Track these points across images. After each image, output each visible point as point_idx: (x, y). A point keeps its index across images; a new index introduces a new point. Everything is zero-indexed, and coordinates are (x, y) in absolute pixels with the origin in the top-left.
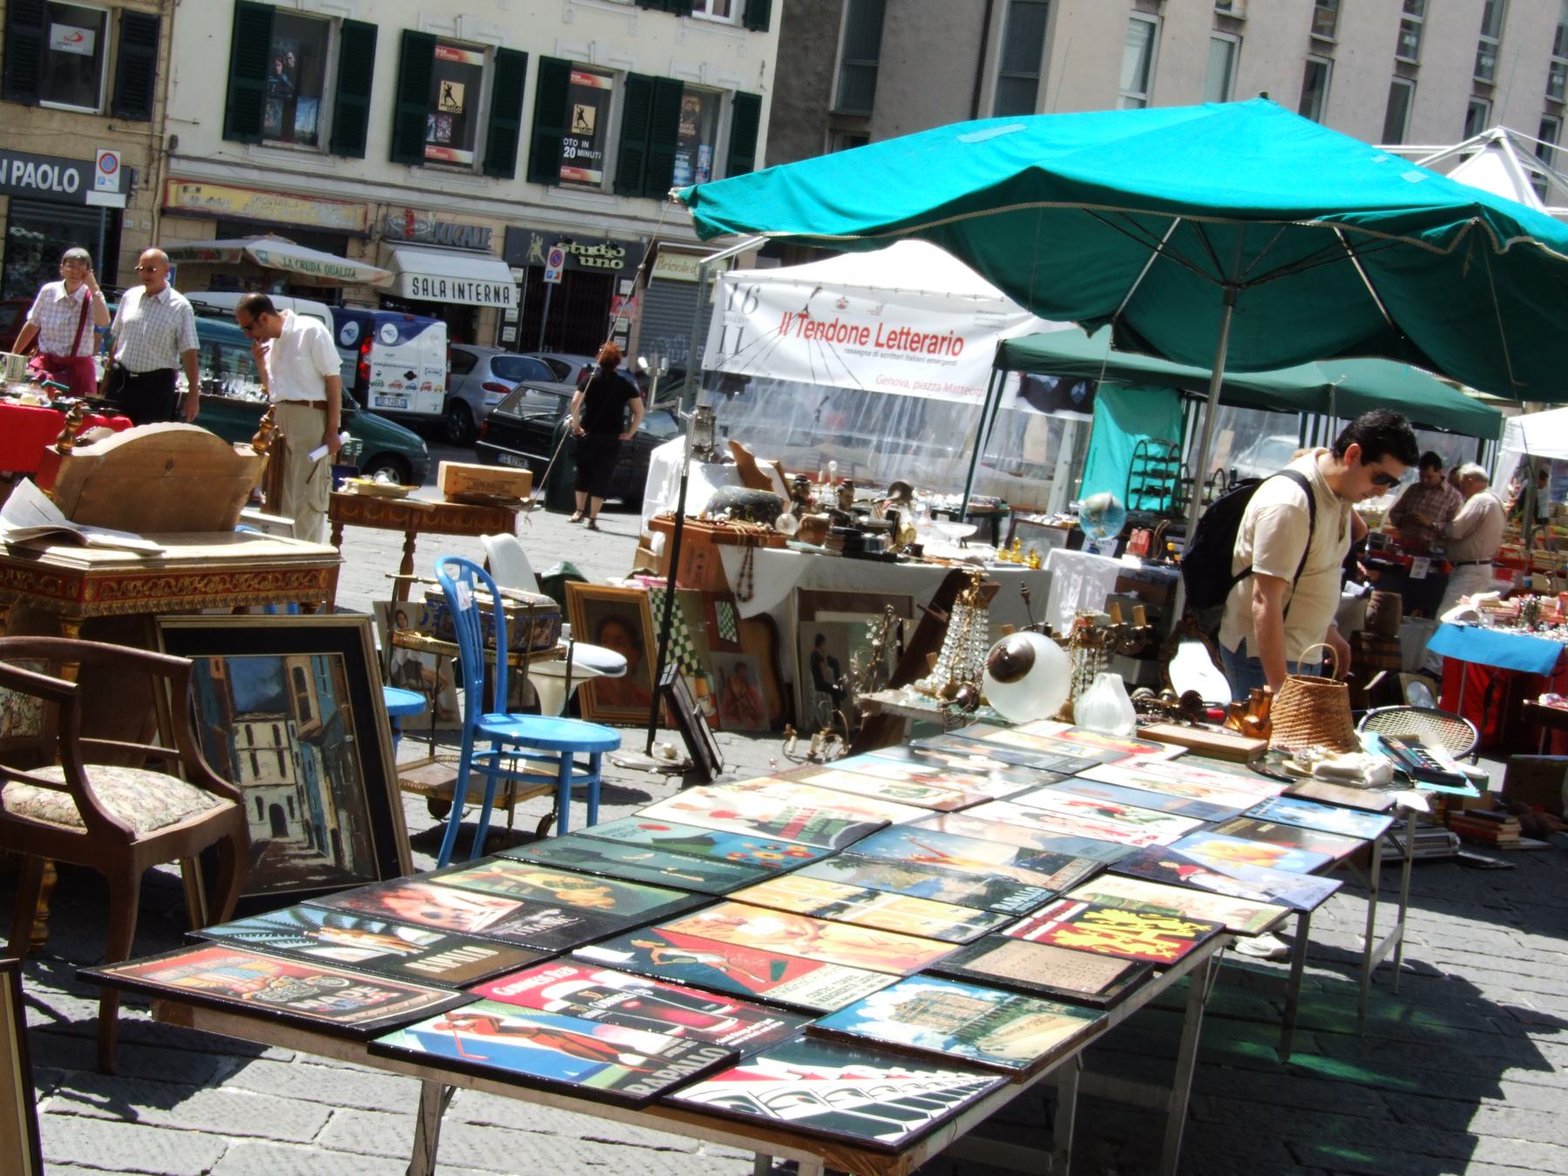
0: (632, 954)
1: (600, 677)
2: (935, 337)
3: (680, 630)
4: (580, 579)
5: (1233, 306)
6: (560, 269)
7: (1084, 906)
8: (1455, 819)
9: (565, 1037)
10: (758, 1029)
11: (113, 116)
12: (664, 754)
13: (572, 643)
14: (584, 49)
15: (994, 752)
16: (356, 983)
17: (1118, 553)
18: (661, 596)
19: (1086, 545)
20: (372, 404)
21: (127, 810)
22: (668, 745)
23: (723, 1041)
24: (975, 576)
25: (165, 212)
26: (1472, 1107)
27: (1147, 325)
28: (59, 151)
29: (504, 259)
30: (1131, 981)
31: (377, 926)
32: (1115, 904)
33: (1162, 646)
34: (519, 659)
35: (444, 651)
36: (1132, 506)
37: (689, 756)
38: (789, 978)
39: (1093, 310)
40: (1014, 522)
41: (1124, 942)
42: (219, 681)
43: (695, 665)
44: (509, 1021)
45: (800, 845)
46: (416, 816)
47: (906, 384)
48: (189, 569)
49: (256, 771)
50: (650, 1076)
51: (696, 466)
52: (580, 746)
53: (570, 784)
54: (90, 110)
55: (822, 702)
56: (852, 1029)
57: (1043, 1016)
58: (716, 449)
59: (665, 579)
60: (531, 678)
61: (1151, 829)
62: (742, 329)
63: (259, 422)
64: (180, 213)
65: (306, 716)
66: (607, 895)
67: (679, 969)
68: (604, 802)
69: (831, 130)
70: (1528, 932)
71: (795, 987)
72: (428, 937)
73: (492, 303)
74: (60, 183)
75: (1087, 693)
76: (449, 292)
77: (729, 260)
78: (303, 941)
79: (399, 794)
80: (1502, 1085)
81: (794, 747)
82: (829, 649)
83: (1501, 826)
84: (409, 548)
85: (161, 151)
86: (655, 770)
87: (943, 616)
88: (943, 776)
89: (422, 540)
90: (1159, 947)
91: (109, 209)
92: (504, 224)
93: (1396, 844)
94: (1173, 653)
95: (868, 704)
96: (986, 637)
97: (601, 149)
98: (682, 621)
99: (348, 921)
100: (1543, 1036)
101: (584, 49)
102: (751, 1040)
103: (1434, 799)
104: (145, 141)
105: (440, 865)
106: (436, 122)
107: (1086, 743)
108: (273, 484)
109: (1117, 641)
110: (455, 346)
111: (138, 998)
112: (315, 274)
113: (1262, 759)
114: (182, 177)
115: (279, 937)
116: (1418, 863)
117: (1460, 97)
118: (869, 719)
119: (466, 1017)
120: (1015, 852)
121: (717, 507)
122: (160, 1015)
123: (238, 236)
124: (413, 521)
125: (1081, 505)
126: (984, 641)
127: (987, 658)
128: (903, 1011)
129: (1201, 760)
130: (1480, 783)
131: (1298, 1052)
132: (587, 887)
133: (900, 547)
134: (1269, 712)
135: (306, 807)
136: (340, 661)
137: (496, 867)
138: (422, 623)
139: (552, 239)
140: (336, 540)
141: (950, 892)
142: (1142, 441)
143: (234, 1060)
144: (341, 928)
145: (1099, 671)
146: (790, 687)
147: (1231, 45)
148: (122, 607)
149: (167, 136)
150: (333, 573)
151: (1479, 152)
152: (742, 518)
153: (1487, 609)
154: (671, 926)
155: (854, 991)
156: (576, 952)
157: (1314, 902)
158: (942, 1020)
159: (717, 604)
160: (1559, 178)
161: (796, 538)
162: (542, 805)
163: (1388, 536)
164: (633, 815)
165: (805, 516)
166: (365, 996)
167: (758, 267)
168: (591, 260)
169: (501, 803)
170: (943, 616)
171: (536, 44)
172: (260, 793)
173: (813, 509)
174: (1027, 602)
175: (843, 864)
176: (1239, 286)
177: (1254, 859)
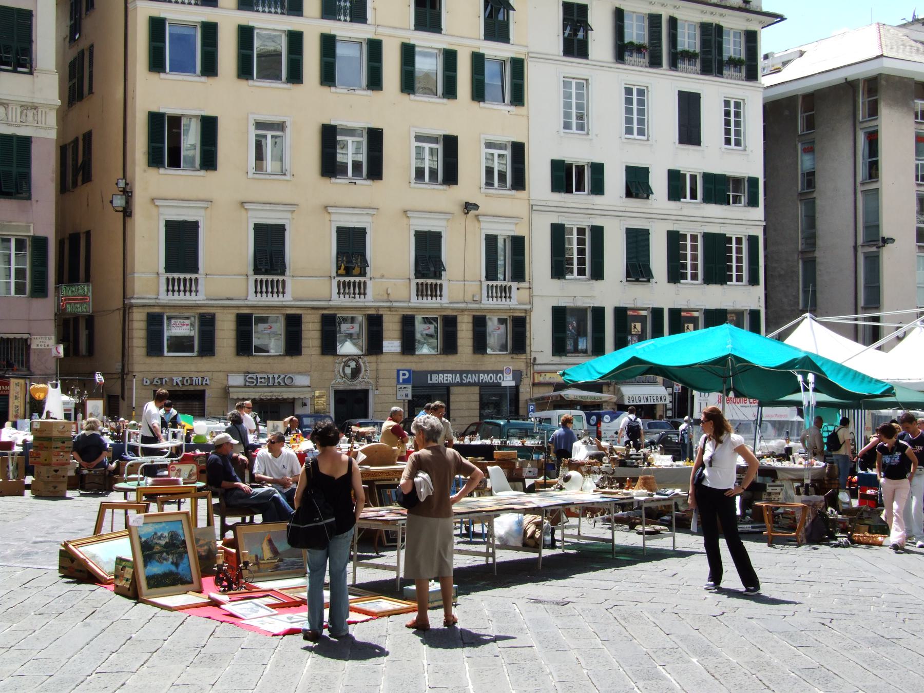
11: (513, 353)
25: (534, 384)
28: (495, 368)
42: (389, 495)
54: (505, 352)
73: (660, 403)
74: (496, 379)
76: (642, 400)
104: (525, 361)
123: (560, 390)
149: (532, 358)
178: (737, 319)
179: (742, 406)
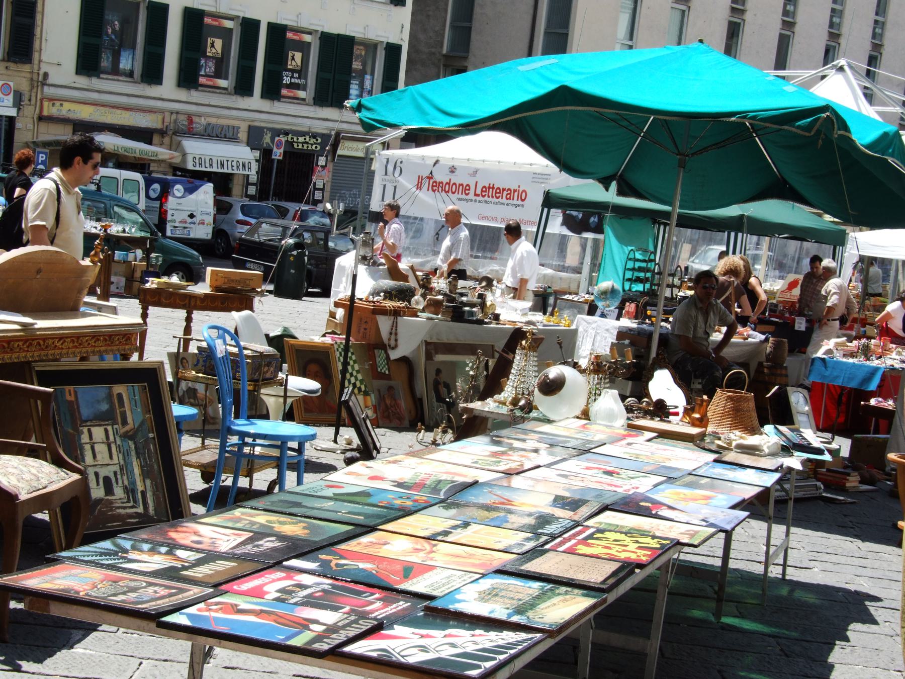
0: (319, 564)
1: (305, 396)
2: (509, 189)
3: (354, 367)
4: (295, 338)
5: (684, 168)
6: (282, 150)
7: (595, 529)
8: (822, 474)
9: (277, 615)
10: (395, 608)
11: (9, 61)
12: (345, 442)
13: (287, 376)
14: (362, 30)
15: (541, 438)
16: (150, 584)
17: (618, 319)
18: (342, 346)
19: (598, 312)
20: (169, 233)
21: (14, 481)
22: (347, 437)
23: (373, 615)
24: (529, 332)
25: (41, 118)
26: (831, 646)
27: (638, 179)
29: (248, 144)
30: (621, 575)
31: (164, 550)
32: (613, 529)
33: (644, 372)
34: (255, 386)
35: (209, 382)
36: (627, 288)
37: (360, 443)
38: (415, 577)
39: (608, 171)
40: (556, 299)
41: (618, 551)
42: (71, 402)
43: (363, 388)
44: (243, 606)
45: (422, 496)
46: (194, 482)
47: (496, 220)
48: (51, 334)
49: (94, 456)
50: (328, 638)
51: (362, 270)
52: (292, 438)
53: (286, 461)
55: (440, 409)
56: (452, 607)
57: (568, 597)
58: (374, 257)
59: (344, 336)
60: (263, 397)
61: (635, 482)
62: (395, 187)
63: (94, 244)
64: (51, 119)
65: (124, 422)
66: (304, 528)
67: (347, 572)
68: (307, 471)
69: (444, 65)
70: (863, 541)
71: (418, 582)
72: (195, 555)
73: (241, 172)
75: (597, 401)
76: (215, 165)
77: (384, 144)
78: (118, 559)
79: (182, 468)
80: (849, 633)
81: (423, 436)
82: (444, 377)
83: (848, 478)
84: (189, 320)
85: (38, 82)
86: (339, 452)
87: (510, 356)
88: (510, 453)
89: (197, 315)
90: (639, 554)
91: (6, 117)
92: (248, 123)
93: (783, 489)
94: (651, 377)
95: (466, 410)
96: (536, 369)
97: (306, 78)
98: (355, 362)
99: (146, 547)
100: (873, 604)
101: (362, 30)
102: (390, 614)
103: (805, 462)
104: (28, 75)
105: (208, 511)
106: (205, 62)
107: (596, 432)
108: (104, 283)
109: (615, 370)
110: (218, 198)
111: (21, 596)
112: (133, 155)
113: (702, 440)
114: (50, 97)
115: (104, 557)
116: (797, 500)
117: (821, 41)
118: (467, 419)
119: (217, 604)
120: (553, 497)
121: (376, 293)
122: (31, 605)
124: (191, 304)
125: (596, 289)
126: (535, 371)
127: (537, 381)
128: (483, 595)
129: (666, 441)
130: (834, 453)
131: (726, 616)
132: (293, 523)
133: (486, 315)
134: (707, 411)
135: (125, 478)
136: (145, 389)
137: (238, 512)
138: (196, 365)
139: (276, 132)
140: (144, 316)
141: (513, 523)
142: (632, 250)
143: (81, 632)
144: (141, 551)
145: (604, 388)
146: (421, 400)
147: (683, 11)
148: (11, 358)
149: (41, 72)
150: (143, 335)
151: (831, 74)
152: (391, 299)
153: (839, 348)
154: (343, 546)
155: (453, 584)
156: (285, 563)
157: (732, 525)
158: (506, 600)
159: (376, 351)
160: (879, 90)
161: (423, 311)
162: (271, 474)
163: (780, 305)
164: (321, 479)
165: (429, 297)
166: (155, 592)
167: (401, 148)
168: (300, 145)
169: (245, 473)
170: (510, 356)
171: (265, 15)
172: (97, 469)
173: (433, 293)
174: (561, 347)
175: (449, 507)
176: (687, 156)
177: (696, 500)
178: (365, 54)
179: (460, 199)
